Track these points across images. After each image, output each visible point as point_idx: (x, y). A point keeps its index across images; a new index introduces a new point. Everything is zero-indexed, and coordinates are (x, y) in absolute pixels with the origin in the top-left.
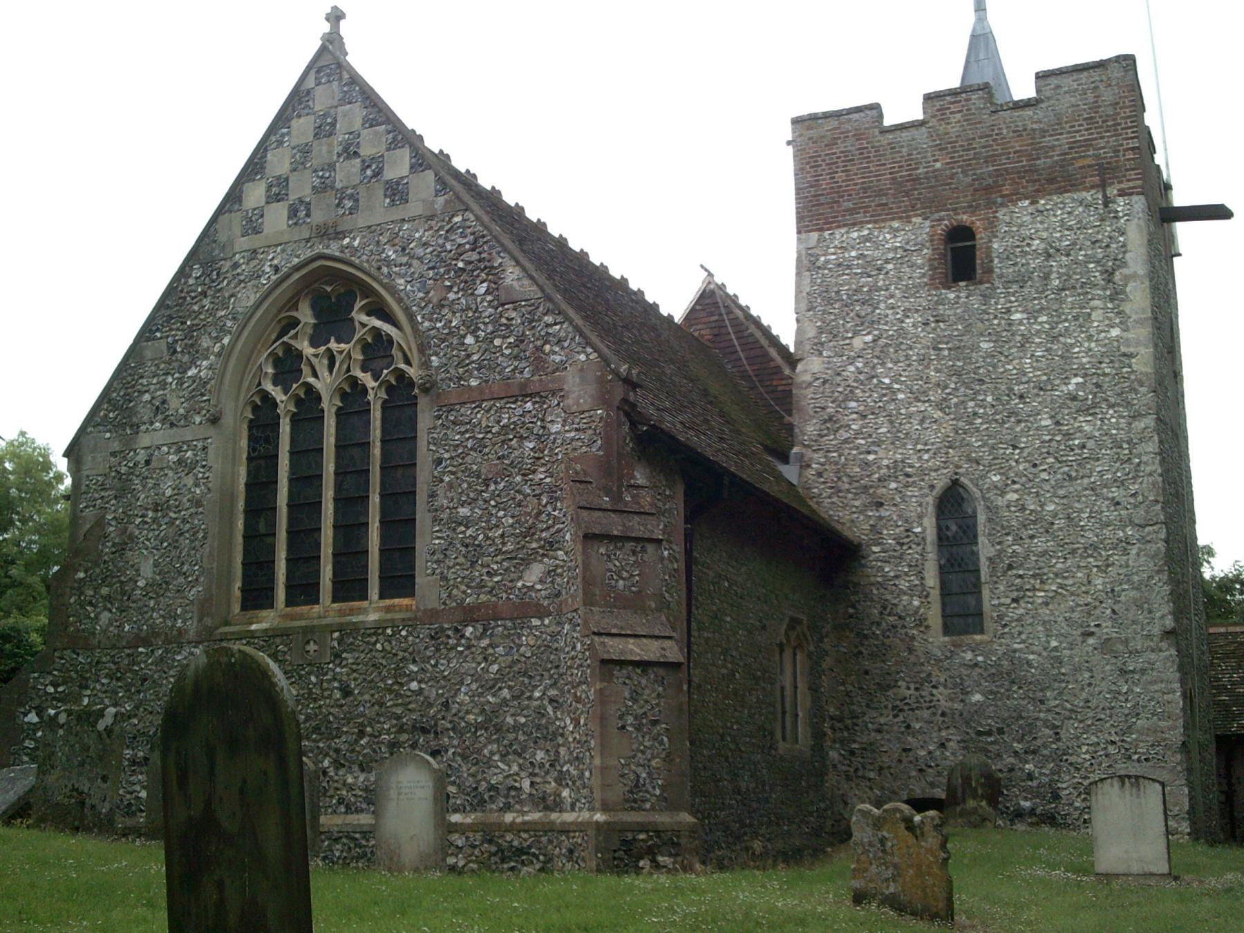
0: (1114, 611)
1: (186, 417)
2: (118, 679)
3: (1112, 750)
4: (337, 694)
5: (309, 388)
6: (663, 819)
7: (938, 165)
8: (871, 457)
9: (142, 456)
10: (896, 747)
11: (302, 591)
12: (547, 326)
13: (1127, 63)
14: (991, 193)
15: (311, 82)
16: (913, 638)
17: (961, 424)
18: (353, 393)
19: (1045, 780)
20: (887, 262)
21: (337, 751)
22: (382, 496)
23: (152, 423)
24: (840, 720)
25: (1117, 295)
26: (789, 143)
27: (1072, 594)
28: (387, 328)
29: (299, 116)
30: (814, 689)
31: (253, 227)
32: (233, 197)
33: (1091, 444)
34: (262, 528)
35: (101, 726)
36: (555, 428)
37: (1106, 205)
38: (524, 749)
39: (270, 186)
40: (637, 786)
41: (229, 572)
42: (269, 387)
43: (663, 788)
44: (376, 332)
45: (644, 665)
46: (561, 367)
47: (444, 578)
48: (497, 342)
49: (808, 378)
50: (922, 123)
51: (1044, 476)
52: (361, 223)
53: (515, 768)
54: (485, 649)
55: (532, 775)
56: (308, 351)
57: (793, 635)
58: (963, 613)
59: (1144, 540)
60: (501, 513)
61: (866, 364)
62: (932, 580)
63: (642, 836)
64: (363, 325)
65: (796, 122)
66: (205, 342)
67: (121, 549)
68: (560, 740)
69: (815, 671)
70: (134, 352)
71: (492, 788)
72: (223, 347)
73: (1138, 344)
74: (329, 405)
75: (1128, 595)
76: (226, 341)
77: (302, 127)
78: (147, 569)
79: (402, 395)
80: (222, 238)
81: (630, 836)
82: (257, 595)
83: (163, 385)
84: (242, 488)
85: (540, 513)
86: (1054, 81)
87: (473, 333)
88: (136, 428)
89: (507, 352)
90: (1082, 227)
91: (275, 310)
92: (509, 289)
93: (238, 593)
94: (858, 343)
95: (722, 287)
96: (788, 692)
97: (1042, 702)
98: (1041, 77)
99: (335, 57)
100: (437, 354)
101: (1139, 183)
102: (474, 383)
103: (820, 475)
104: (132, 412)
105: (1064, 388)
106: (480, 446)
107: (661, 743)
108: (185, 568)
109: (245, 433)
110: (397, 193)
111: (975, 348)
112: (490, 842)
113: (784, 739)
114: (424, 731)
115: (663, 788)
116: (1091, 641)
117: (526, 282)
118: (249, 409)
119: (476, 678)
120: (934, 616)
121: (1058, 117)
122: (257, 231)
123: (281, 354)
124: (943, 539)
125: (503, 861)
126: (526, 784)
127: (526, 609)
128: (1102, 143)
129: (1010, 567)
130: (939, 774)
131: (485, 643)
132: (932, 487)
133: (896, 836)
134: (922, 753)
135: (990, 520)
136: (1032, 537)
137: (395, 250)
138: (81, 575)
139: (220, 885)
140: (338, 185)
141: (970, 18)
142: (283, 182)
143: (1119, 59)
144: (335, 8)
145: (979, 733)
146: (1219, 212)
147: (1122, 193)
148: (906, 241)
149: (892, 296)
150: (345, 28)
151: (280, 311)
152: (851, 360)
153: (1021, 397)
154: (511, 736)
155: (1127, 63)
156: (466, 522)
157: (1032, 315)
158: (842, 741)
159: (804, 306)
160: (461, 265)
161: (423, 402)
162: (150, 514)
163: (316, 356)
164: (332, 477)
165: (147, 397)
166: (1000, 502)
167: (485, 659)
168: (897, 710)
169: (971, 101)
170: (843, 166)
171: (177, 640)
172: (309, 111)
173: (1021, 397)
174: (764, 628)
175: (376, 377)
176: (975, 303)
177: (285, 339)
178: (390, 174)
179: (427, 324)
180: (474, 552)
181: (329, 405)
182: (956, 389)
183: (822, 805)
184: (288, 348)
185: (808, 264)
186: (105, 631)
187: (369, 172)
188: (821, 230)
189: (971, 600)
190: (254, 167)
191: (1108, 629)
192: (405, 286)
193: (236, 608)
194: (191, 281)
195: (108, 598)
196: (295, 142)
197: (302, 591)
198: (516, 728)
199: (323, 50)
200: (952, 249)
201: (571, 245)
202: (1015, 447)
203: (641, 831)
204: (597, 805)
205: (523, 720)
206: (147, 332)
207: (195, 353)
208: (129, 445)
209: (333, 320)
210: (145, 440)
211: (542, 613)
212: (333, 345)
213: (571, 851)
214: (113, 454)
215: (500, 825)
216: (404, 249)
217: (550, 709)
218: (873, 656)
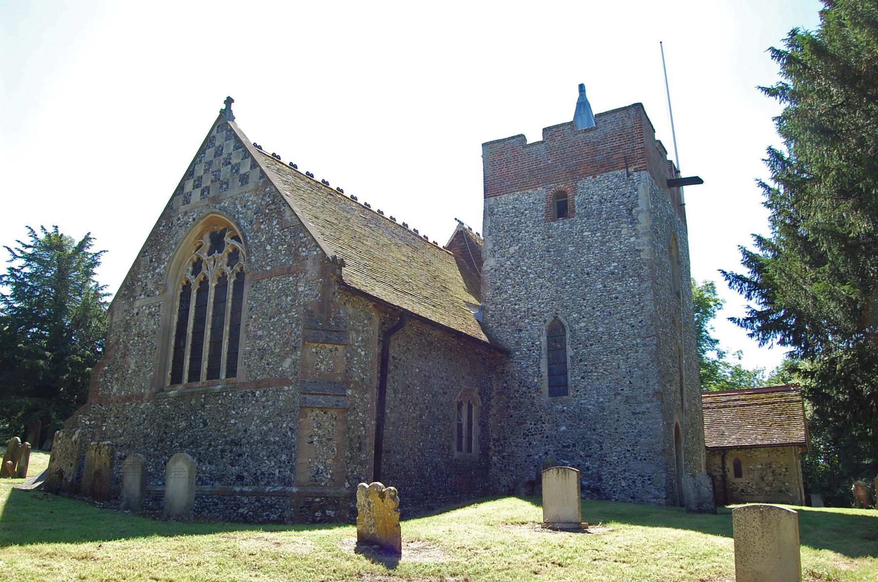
0: (630, 383)
3: (628, 455)
4: (202, 426)
7: (550, 162)
8: (517, 307)
9: (136, 311)
10: (524, 455)
11: (195, 375)
14: (574, 174)
15: (215, 133)
16: (534, 398)
17: (559, 288)
21: (200, 454)
25: (633, 221)
27: (610, 374)
31: (187, 201)
33: (620, 296)
36: (300, 289)
37: (628, 176)
38: (277, 453)
40: (317, 473)
43: (332, 475)
47: (249, 366)
48: (280, 247)
49: (488, 268)
50: (542, 142)
52: (229, 195)
58: (558, 385)
59: (645, 345)
62: (544, 369)
65: (483, 145)
67: (124, 356)
73: (644, 245)
74: (212, 285)
75: (638, 373)
77: (210, 152)
78: (133, 366)
79: (240, 276)
82: (176, 378)
83: (147, 277)
84: (175, 325)
85: (291, 333)
90: (617, 188)
93: (169, 376)
94: (512, 250)
97: (594, 430)
101: (704, 400)
103: (492, 316)
104: (134, 290)
105: (782, 191)
106: (269, 300)
109: (178, 298)
110: (244, 179)
111: (566, 250)
112: (258, 501)
113: (460, 449)
114: (236, 444)
115: (332, 475)
116: (619, 398)
119: (259, 417)
120: (545, 387)
121: (605, 135)
122: (188, 203)
124: (551, 349)
125: (264, 511)
126: (277, 471)
129: (581, 360)
131: (264, 399)
132: (545, 321)
135: (572, 337)
136: (591, 345)
137: (241, 200)
143: (519, 136)
144: (229, 98)
145: (564, 447)
150: (234, 107)
152: (508, 259)
153: (588, 274)
154: (272, 447)
156: (260, 338)
157: (594, 232)
158: (499, 453)
164: (212, 305)
165: (140, 283)
166: (576, 327)
171: (140, 397)
173: (588, 274)
174: (445, 393)
178: (243, 171)
181: (212, 285)
182: (557, 271)
183: (486, 484)
186: (115, 394)
189: (562, 378)
190: (190, 173)
191: (627, 392)
193: (168, 383)
195: (117, 379)
198: (274, 443)
202: (584, 299)
203: (317, 497)
205: (277, 439)
207: (159, 261)
208: (131, 305)
209: (217, 243)
210: (137, 304)
211: (289, 383)
215: (263, 492)
217: (289, 433)
218: (515, 408)
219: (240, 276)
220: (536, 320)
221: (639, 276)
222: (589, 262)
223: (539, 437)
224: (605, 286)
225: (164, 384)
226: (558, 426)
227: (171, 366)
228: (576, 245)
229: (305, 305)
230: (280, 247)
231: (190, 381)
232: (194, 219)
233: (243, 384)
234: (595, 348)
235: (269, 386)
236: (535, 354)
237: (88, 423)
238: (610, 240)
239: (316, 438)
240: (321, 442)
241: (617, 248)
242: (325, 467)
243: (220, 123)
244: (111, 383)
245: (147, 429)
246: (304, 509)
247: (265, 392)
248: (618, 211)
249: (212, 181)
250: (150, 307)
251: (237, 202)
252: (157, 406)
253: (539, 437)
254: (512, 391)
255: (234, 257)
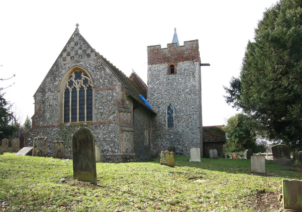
1: (54, 91)
2: (44, 133)
3: (190, 144)
5: (74, 87)
6: (131, 154)
7: (169, 55)
9: (47, 97)
10: (160, 144)
11: (74, 119)
12: (113, 78)
13: (197, 41)
18: (82, 89)
19: (181, 148)
20: (161, 70)
22: (87, 105)
23: (48, 92)
24: (153, 140)
25: (194, 77)
26: (34, 104)
28: (87, 78)
29: (72, 42)
30: (149, 135)
31: (64, 60)
32: (61, 55)
33: (190, 99)
34: (67, 109)
35: (44, 140)
36: (114, 95)
37: (193, 63)
38: (110, 144)
39: (67, 53)
41: (62, 116)
42: (68, 86)
44: (86, 79)
45: (128, 131)
46: (116, 85)
47: (97, 118)
50: (167, 48)
51: (183, 104)
53: (108, 147)
54: (104, 129)
55: (111, 148)
56: (74, 81)
57: (146, 127)
58: (171, 125)
60: (106, 108)
61: (158, 86)
62: (167, 119)
63: (128, 157)
64: (83, 77)
65: (148, 47)
66: (57, 79)
67: (44, 112)
68: (115, 143)
69: (149, 133)
70: (45, 80)
71: (105, 150)
72: (60, 80)
74: (78, 90)
76: (60, 79)
77: (72, 44)
78: (48, 116)
79: (90, 89)
80: (59, 62)
81: (126, 156)
82: (66, 120)
84: (64, 103)
86: (187, 43)
87: (101, 79)
88: (46, 93)
89: (107, 82)
90: (190, 66)
91: (68, 74)
92: (107, 72)
93: (63, 120)
95: (135, 73)
96: (146, 136)
98: (185, 42)
99: (78, 32)
100: (95, 82)
102: (102, 87)
106: (103, 97)
107: (131, 143)
108: (55, 115)
109: (64, 94)
110: (89, 56)
111: (174, 84)
112: (105, 158)
115: (131, 150)
117: (110, 71)
118: (64, 90)
119: (102, 133)
120: (167, 125)
121: (187, 49)
122: (65, 61)
123: (88, 86)
125: (107, 160)
126: (110, 149)
127: (110, 122)
128: (193, 53)
129: (178, 117)
130: (166, 148)
131: (103, 128)
133: (167, 155)
134: (164, 145)
136: (181, 113)
137: (86, 64)
138: (37, 116)
139: (82, 162)
140: (79, 54)
141: (174, 31)
142: (69, 53)
143: (196, 40)
144: (77, 24)
145: (172, 142)
146: (208, 65)
147: (196, 61)
148: (164, 67)
149: (162, 76)
151: (69, 74)
152: (156, 85)
154: (108, 142)
155: (197, 41)
156: (100, 109)
157: (182, 79)
159: (149, 76)
160: (99, 68)
161: (93, 90)
162: (48, 107)
163: (76, 82)
165: (47, 87)
166: (176, 107)
167: (104, 130)
168: (161, 139)
169: (173, 45)
170: (155, 55)
172: (74, 41)
175: (85, 86)
176: (174, 77)
177: (70, 79)
178: (87, 52)
179: (94, 77)
180: (102, 114)
181: (78, 90)
184: (71, 81)
185: (150, 70)
187: (84, 52)
188: (152, 64)
189: (172, 122)
190: (64, 50)
191: (190, 127)
192: (89, 71)
193: (63, 122)
194: (54, 69)
195: (42, 120)
196: (71, 46)
197: (74, 119)
198: (108, 141)
199: (76, 31)
200: (171, 69)
201: (107, 60)
204: (121, 152)
206: (47, 77)
207: (55, 80)
208: (44, 95)
209: (78, 76)
210: (47, 95)
211: (112, 123)
212: (78, 80)
213: (117, 159)
214: (42, 97)
215: (106, 155)
216: (90, 65)
219: (90, 89)
220: (164, 105)
221: (195, 94)
222: (181, 88)
223: (165, 139)
224: (185, 96)
225: (62, 122)
226: (170, 136)
227: (64, 116)
228: (177, 83)
229: (117, 100)
230: (105, 81)
231: (72, 121)
232: (69, 67)
233: (95, 123)
234: (182, 114)
235: (105, 124)
236: (164, 115)
237: (33, 135)
238: (187, 82)
239: (126, 140)
240: (127, 141)
241: (189, 85)
242: (129, 148)
243: (75, 33)
244: (40, 121)
245: (58, 137)
246: (125, 159)
247: (104, 126)
248: (190, 73)
249: (75, 55)
250: (53, 96)
251: (86, 63)
252: (61, 129)
253: (165, 139)
254: (157, 126)
255: (86, 81)
